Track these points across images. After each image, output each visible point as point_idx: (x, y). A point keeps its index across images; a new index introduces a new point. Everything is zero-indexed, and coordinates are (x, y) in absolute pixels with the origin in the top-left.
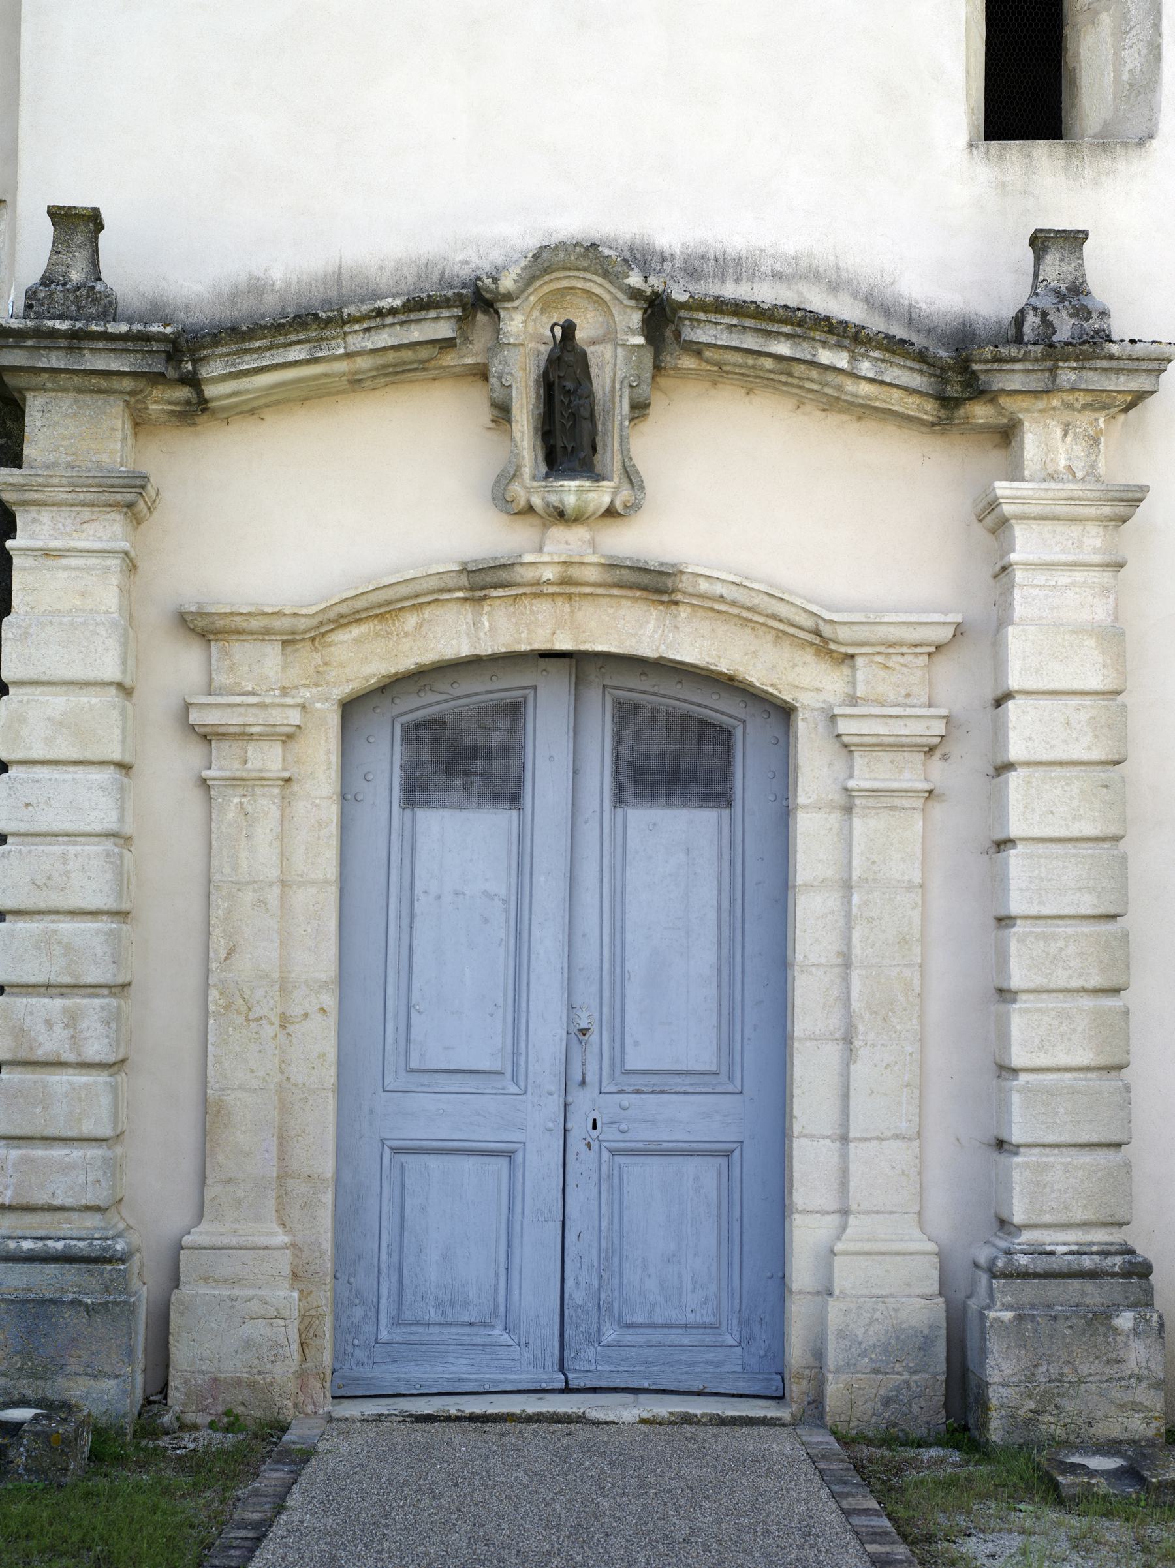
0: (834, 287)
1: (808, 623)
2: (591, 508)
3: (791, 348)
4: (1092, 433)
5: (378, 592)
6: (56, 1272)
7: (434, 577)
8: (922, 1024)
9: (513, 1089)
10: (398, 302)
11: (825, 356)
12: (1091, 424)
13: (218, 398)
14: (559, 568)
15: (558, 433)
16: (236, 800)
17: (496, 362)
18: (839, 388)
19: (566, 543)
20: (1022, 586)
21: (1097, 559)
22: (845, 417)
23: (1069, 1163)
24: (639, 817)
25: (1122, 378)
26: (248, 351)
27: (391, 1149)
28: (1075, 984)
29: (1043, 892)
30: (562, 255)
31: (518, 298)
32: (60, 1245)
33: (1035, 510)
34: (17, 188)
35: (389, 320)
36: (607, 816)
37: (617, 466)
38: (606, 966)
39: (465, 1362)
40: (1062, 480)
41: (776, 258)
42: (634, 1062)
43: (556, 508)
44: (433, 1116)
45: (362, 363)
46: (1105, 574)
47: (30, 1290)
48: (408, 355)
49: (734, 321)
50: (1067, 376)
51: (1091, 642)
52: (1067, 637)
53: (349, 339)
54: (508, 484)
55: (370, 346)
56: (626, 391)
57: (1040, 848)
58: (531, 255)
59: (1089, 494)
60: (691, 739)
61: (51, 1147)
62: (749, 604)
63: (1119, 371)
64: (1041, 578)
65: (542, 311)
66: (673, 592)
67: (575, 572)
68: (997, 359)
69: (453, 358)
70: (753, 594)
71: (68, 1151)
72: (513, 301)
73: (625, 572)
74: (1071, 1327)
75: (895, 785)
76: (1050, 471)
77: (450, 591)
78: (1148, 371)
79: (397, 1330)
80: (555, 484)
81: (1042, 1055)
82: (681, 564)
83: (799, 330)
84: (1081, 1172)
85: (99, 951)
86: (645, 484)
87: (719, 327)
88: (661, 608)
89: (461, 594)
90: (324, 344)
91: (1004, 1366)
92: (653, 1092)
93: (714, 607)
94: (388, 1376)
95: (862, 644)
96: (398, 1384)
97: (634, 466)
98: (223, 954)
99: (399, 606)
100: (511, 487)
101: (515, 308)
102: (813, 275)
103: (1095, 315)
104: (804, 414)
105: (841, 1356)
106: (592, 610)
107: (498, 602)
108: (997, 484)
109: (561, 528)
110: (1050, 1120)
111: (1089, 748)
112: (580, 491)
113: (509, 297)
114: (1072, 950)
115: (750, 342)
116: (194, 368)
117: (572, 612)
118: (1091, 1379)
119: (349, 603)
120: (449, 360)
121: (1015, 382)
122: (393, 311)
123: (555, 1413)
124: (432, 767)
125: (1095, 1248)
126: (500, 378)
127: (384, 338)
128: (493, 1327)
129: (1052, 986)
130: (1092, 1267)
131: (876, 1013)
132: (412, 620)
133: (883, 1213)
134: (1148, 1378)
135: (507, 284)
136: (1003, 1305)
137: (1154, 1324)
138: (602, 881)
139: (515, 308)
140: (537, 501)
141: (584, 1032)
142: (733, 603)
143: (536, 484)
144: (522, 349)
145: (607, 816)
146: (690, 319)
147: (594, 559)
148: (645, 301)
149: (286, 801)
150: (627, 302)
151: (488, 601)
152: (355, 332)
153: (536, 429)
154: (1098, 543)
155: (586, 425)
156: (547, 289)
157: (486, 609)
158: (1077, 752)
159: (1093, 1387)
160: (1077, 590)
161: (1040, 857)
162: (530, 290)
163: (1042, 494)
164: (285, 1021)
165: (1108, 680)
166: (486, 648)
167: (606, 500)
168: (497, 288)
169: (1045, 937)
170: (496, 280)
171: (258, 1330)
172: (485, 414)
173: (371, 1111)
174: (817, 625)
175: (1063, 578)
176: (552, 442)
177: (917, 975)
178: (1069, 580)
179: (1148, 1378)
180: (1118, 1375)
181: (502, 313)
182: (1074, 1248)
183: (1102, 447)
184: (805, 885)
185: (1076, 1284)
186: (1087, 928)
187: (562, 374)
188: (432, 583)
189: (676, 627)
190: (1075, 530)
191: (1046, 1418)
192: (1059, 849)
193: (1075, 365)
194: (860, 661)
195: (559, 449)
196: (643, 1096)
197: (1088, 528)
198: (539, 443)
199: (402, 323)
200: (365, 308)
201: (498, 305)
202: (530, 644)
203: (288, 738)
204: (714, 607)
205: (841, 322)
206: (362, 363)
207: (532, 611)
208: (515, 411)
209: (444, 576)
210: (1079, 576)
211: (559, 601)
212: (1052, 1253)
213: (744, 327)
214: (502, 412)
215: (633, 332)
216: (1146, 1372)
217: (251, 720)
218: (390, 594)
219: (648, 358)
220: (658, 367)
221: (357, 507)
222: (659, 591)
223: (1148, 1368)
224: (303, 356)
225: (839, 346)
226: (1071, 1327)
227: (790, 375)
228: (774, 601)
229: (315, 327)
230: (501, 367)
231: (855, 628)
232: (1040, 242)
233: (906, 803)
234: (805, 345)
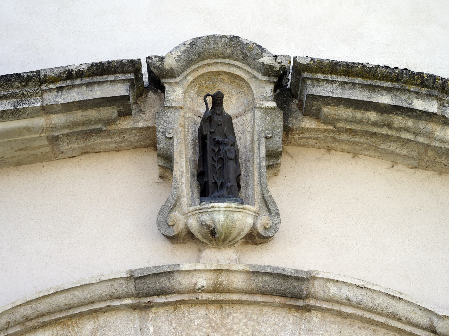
3: (392, 99)
5: (58, 297)
7: (106, 284)
14: (210, 276)
15: (209, 171)
17: (162, 121)
18: (430, 135)
22: (429, 173)
30: (212, 44)
31: (178, 75)
35: (78, 81)
37: (257, 195)
43: (208, 226)
49: (346, 79)
53: (46, 96)
54: (170, 212)
56: (263, 141)
58: (188, 43)
62: (372, 305)
66: (307, 297)
67: (225, 279)
69: (128, 123)
70: (375, 295)
72: (175, 78)
73: (267, 278)
77: (120, 298)
80: (207, 206)
82: (313, 271)
83: (397, 85)
86: (280, 212)
87: (334, 85)
88: (296, 314)
89: (129, 301)
90: (25, 100)
97: (271, 196)
99: (77, 311)
100: (172, 214)
101: (177, 83)
104: (398, 171)
106: (239, 316)
107: (161, 310)
109: (213, 250)
112: (228, 211)
117: (223, 318)
119: (33, 305)
126: (164, 133)
127: (73, 96)
135: (170, 63)
139: (177, 83)
140: (193, 223)
142: (358, 306)
143: (192, 208)
144: (182, 112)
146: (312, 79)
147: (240, 267)
148: (275, 76)
150: (261, 77)
151: (153, 310)
152: (50, 90)
153: (192, 174)
155: (232, 164)
156: (201, 72)
157: (151, 316)
162: (188, 71)
167: (250, 221)
168: (162, 64)
172: (155, 172)
174: (431, 322)
176: (205, 180)
181: (167, 87)
187: (212, 131)
188: (105, 290)
189: (309, 330)
195: (210, 183)
198: (195, 184)
199: (88, 85)
201: (163, 80)
205: (431, 76)
206: (58, 119)
207: (189, 317)
208: (176, 156)
209: (115, 283)
211: (212, 309)
213: (353, 83)
214: (167, 160)
215: (267, 99)
219: (279, 117)
220: (287, 130)
225: (429, 96)
227: (390, 126)
228: (393, 302)
229: (18, 84)
230: (165, 125)
234: (402, 97)
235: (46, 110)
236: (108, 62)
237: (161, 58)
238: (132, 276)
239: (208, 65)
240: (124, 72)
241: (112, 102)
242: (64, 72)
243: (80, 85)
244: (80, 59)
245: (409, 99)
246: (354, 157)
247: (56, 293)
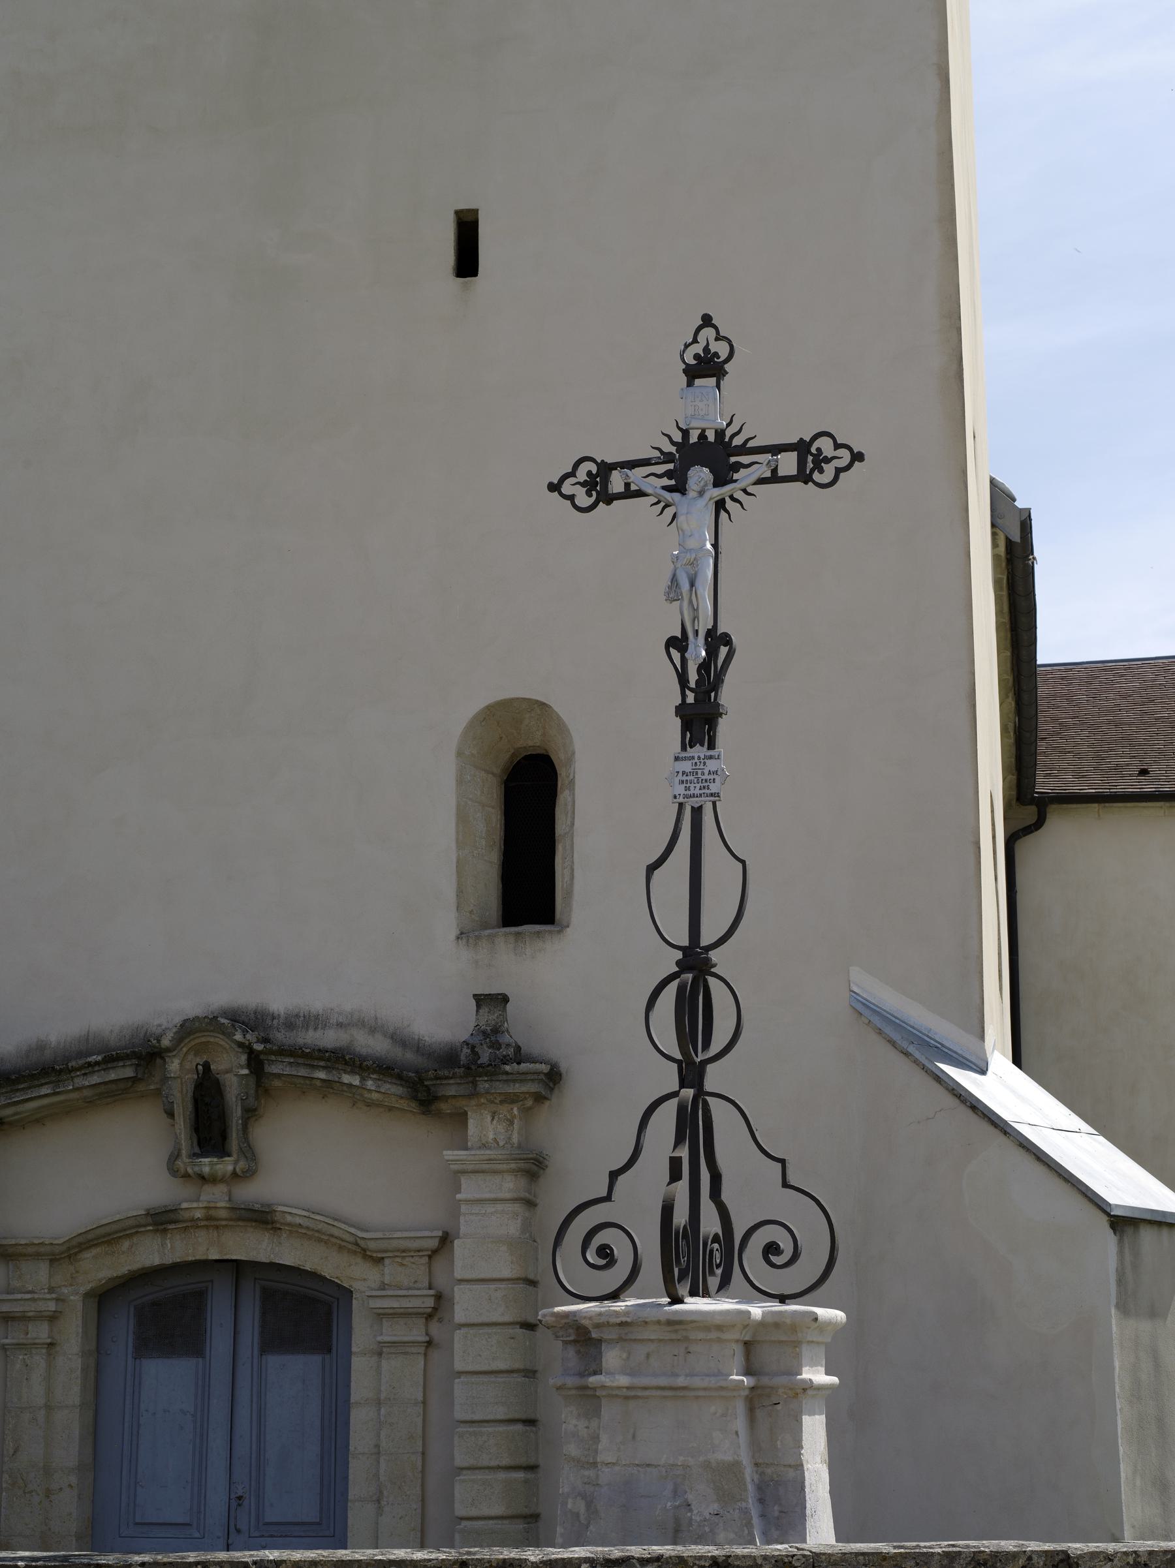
0: (373, 1030)
1: (352, 1239)
2: (220, 1173)
8: (423, 1491)
9: (197, 1535)
10: (99, 1058)
11: (346, 1078)
13: (8, 1116)
14: (203, 1211)
19: (216, 1196)
20: (465, 1214)
21: (508, 1195)
24: (273, 1361)
25: (517, 1085)
26: (18, 1090)
28: (493, 1463)
33: (470, 1167)
34: (529, 700)
35: (97, 1068)
36: (255, 1361)
38: (254, 1456)
40: (490, 1148)
41: (340, 1014)
42: (270, 1516)
45: (86, 1093)
48: (114, 1087)
50: (483, 1086)
51: (504, 1248)
53: (76, 1080)
55: (87, 1084)
57: (474, 1379)
60: (304, 1314)
63: (514, 1081)
64: (476, 1209)
65: (195, 1055)
67: (213, 1213)
68: (437, 1078)
75: (406, 1339)
78: (532, 1080)
93: (297, 1231)
95: (386, 1251)
98: (11, 1452)
102: (361, 1023)
108: (445, 1152)
113: (168, 1050)
115: (303, 1072)
120: (141, 1087)
121: (452, 1091)
122: (97, 1063)
127: (95, 1079)
129: (480, 1465)
132: (126, 1244)
135: (166, 1042)
140: (190, 1170)
141: (240, 1498)
142: (308, 1228)
145: (255, 1361)
154: (511, 1185)
156: (193, 1043)
158: (496, 1317)
164: (48, 1493)
166: (169, 1260)
167: (230, 1168)
170: (159, 1041)
175: (490, 1209)
177: (420, 1458)
186: (502, 1428)
192: (485, 1379)
194: (387, 1261)
200: (81, 1062)
203: (53, 1318)
204: (297, 1231)
206: (86, 1093)
210: (499, 1207)
214: (171, 1114)
215: (242, 1067)
217: (27, 1309)
218: (107, 1229)
221: (104, 1175)
222: (266, 1222)
224: (49, 1091)
232: (481, 1000)
233: (414, 1350)
238: (148, 1214)
241: (126, 1066)
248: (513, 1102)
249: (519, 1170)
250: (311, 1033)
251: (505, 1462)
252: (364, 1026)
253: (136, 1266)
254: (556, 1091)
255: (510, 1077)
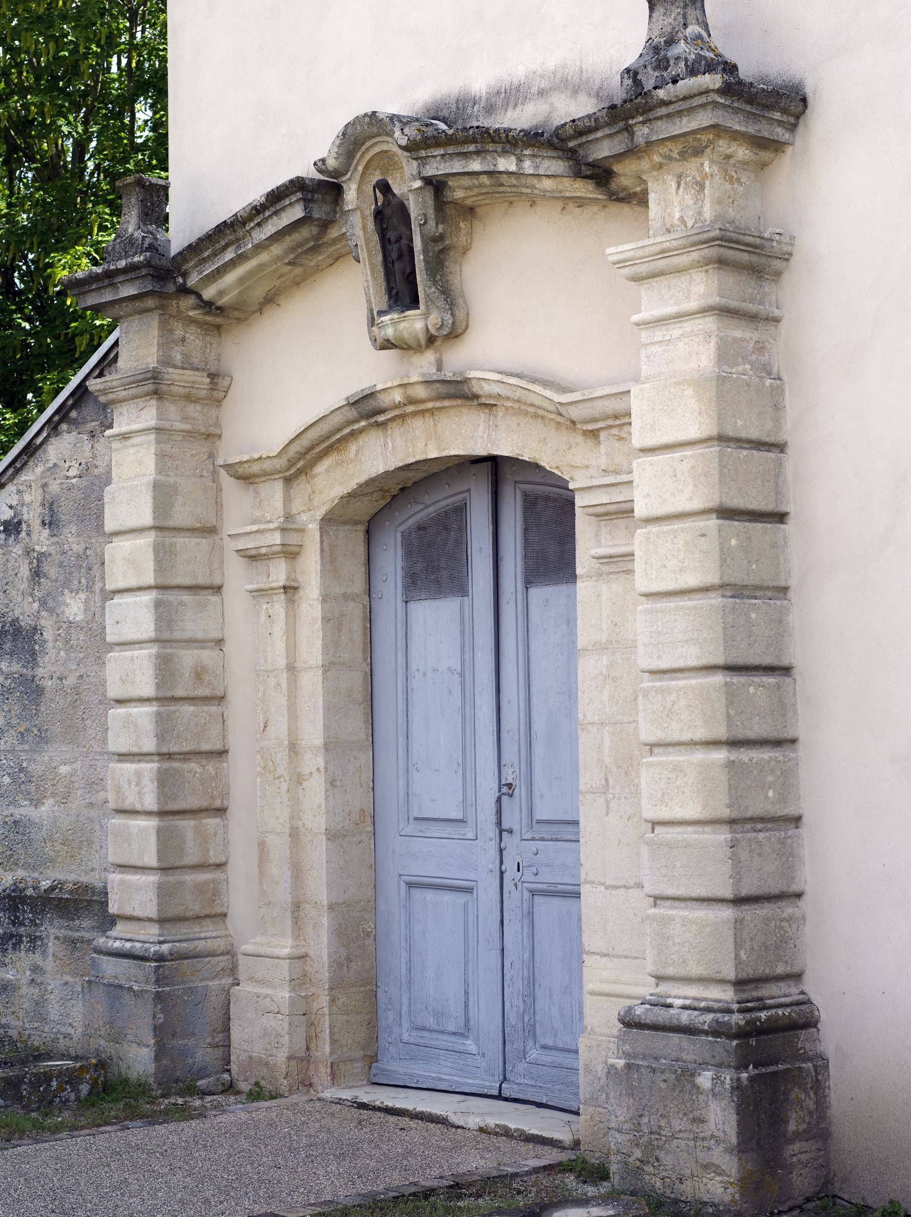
4: (698, 179)
5: (312, 430)
6: (126, 965)
12: (698, 170)
16: (264, 607)
18: (533, 187)
20: (645, 345)
23: (686, 917)
24: (537, 593)
25: (685, 120)
27: (407, 883)
28: (686, 737)
29: (660, 646)
32: (128, 945)
35: (267, 214)
39: (448, 1064)
41: (542, 76)
42: (540, 815)
44: (430, 856)
46: (707, 319)
47: (116, 978)
50: (642, 133)
51: (689, 392)
52: (672, 390)
59: (675, 243)
61: (128, 873)
63: (680, 113)
64: (659, 334)
71: (139, 877)
74: (665, 1081)
75: (241, 531)
76: (668, 226)
78: (703, 106)
79: (414, 1033)
81: (664, 809)
84: (694, 927)
85: (148, 728)
88: (486, 411)
91: (619, 1113)
92: (551, 840)
94: (401, 1070)
96: (405, 1077)
101: (349, 179)
103: (672, 62)
105: (588, 1089)
110: (670, 874)
111: (691, 499)
114: (682, 703)
116: (185, 281)
118: (681, 1135)
123: (430, 1114)
124: (419, 566)
125: (703, 1004)
127: (270, 229)
128: (467, 1037)
129: (669, 739)
130: (687, 1023)
131: (620, 767)
133: (629, 957)
134: (724, 1142)
135: (332, 163)
136: (624, 1052)
137: (728, 1087)
138: (517, 654)
149: (291, 602)
157: (390, 431)
159: (683, 1144)
160: (687, 340)
161: (657, 611)
162: (355, 162)
163: (640, 253)
165: (704, 427)
167: (419, 325)
169: (662, 691)
171: (269, 1021)
173: (393, 851)
175: (675, 331)
178: (680, 332)
179: (724, 1142)
180: (702, 1135)
182: (687, 1002)
183: (706, 191)
184: (583, 649)
185: (675, 1037)
190: (684, 279)
191: (649, 1169)
193: (641, 119)
194: (603, 435)
196: (546, 843)
197: (694, 275)
199: (276, 213)
202: (414, 457)
209: (343, 410)
210: (687, 326)
212: (670, 1006)
216: (722, 1135)
223: (724, 1132)
225: (505, 152)
226: (665, 1081)
231: (580, 406)
235: (260, 247)
236: (278, 188)
237: (323, 160)
239: (371, 146)
240: (293, 193)
242: (252, 209)
243: (270, 216)
244: (256, 194)
245: (494, 158)
246: (531, 206)
247: (306, 429)
248: (698, 152)
249: (707, 262)
250: (510, 113)
251: (700, 734)
252: (566, 87)
253: (363, 478)
254: (800, 128)
255: (671, 109)
